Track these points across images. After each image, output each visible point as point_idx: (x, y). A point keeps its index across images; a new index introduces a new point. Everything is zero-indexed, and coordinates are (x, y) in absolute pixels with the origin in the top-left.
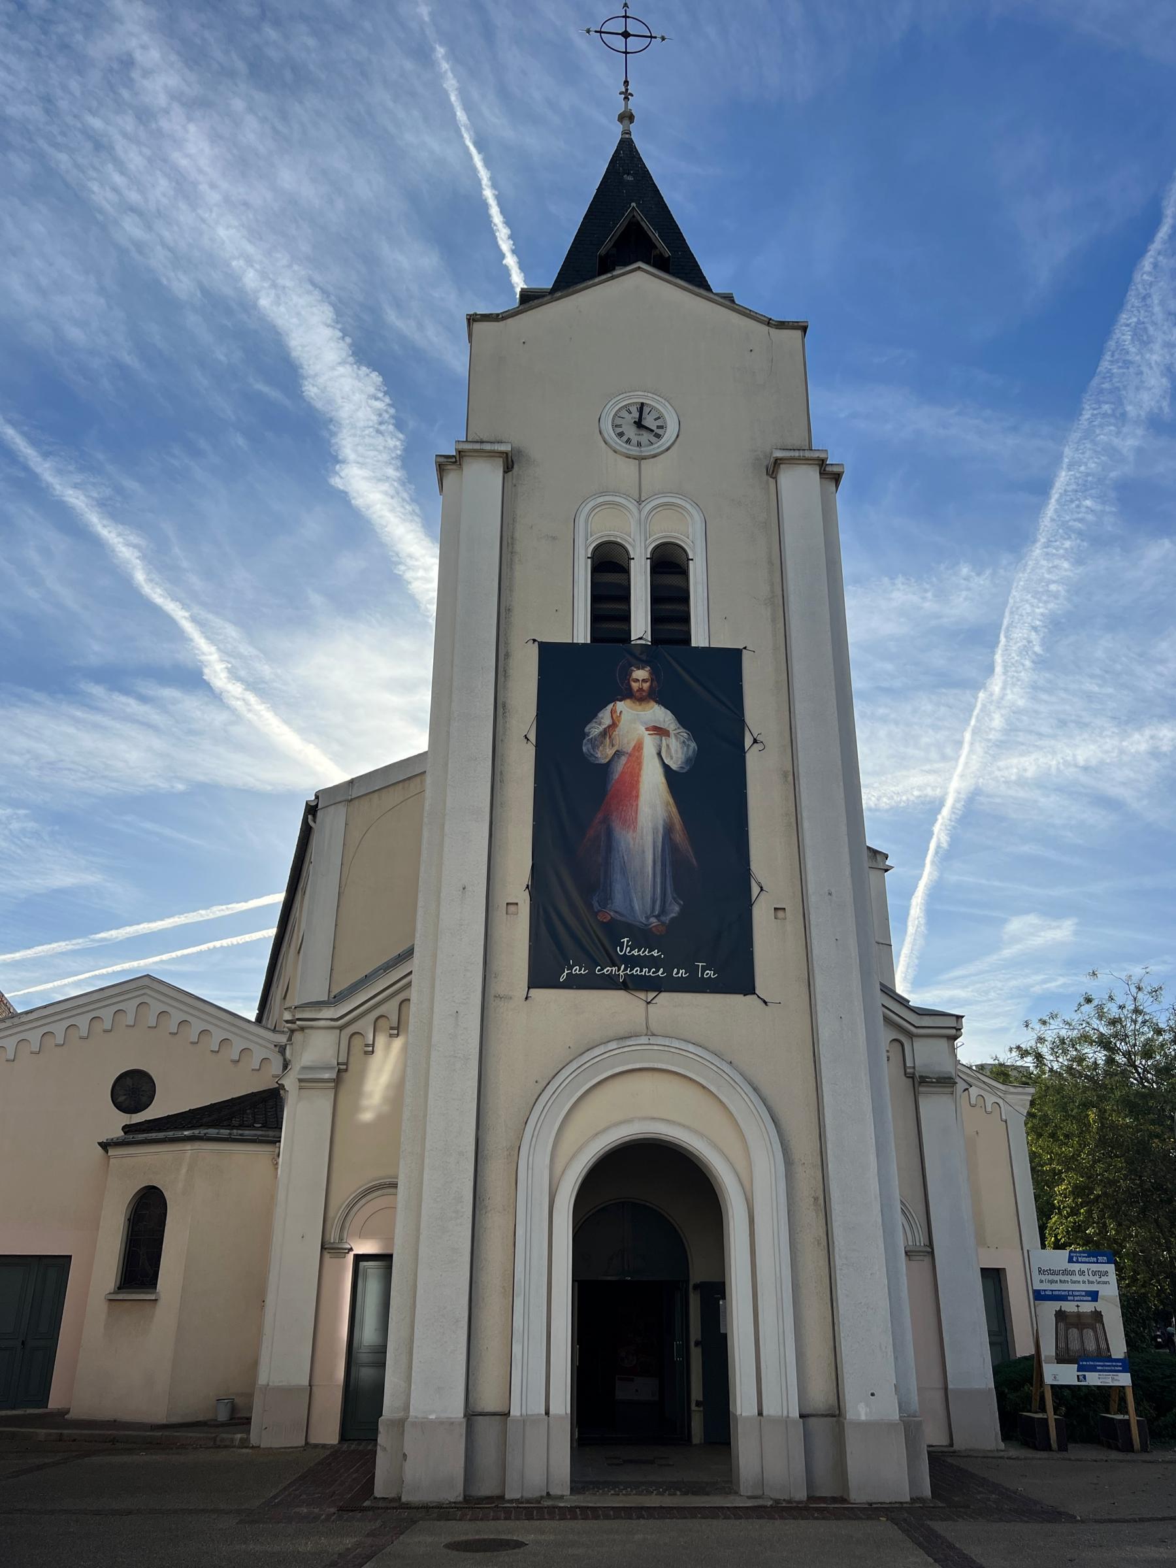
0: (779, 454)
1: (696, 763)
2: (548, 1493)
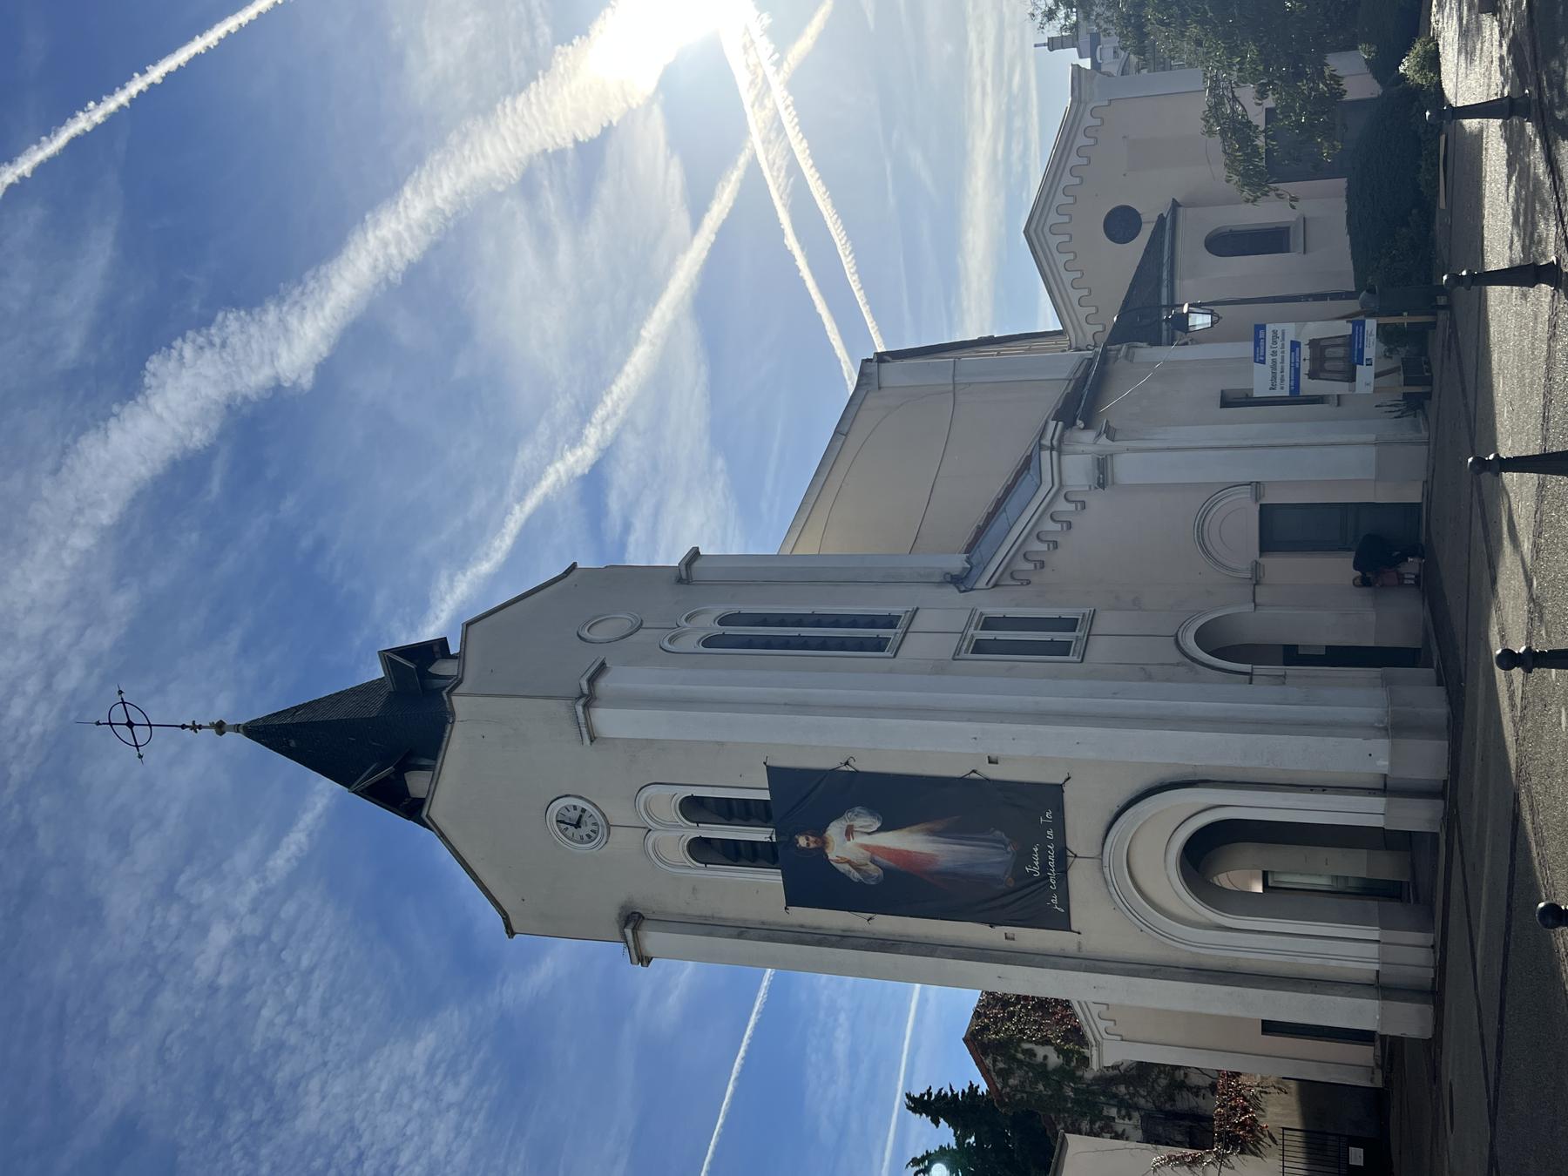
0: (587, 741)
1: (873, 808)
2: (1432, 992)
